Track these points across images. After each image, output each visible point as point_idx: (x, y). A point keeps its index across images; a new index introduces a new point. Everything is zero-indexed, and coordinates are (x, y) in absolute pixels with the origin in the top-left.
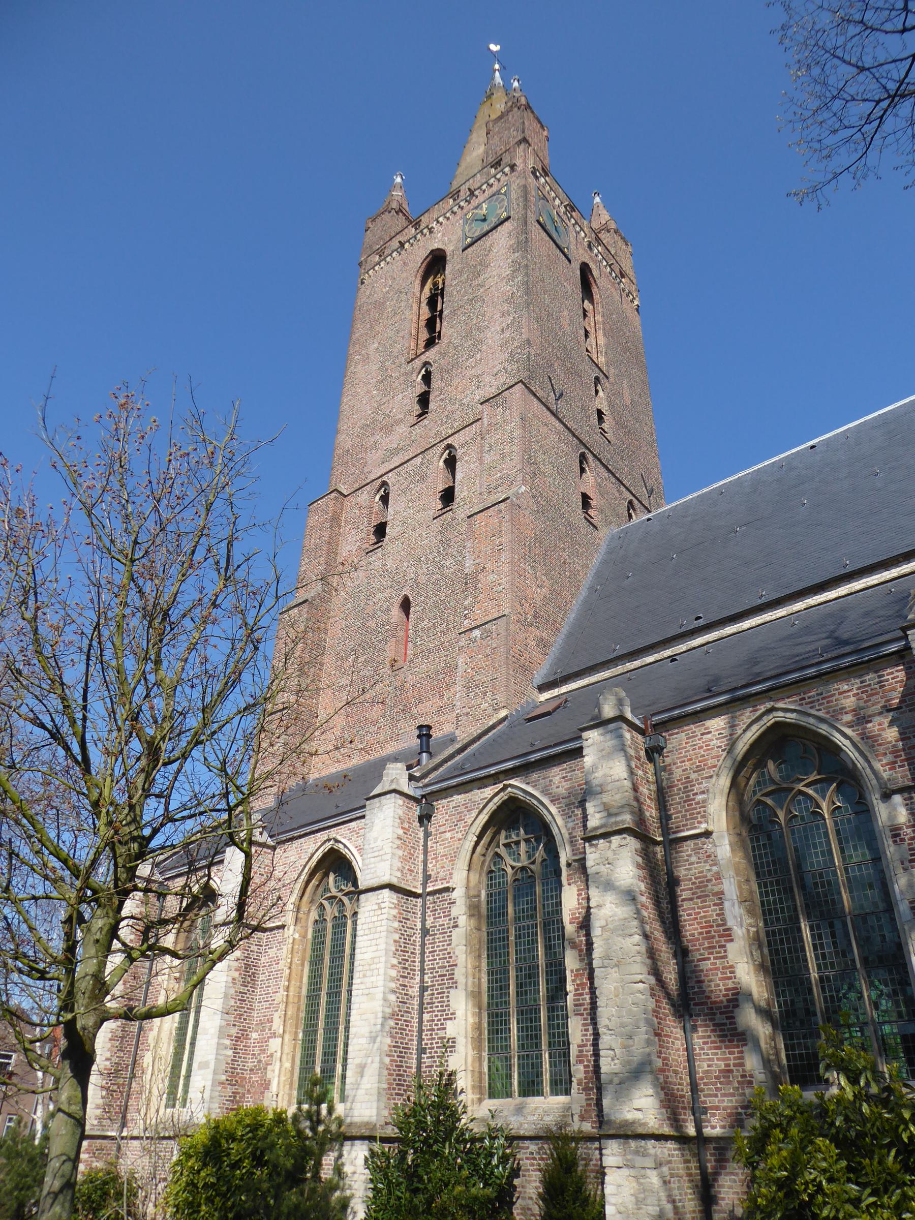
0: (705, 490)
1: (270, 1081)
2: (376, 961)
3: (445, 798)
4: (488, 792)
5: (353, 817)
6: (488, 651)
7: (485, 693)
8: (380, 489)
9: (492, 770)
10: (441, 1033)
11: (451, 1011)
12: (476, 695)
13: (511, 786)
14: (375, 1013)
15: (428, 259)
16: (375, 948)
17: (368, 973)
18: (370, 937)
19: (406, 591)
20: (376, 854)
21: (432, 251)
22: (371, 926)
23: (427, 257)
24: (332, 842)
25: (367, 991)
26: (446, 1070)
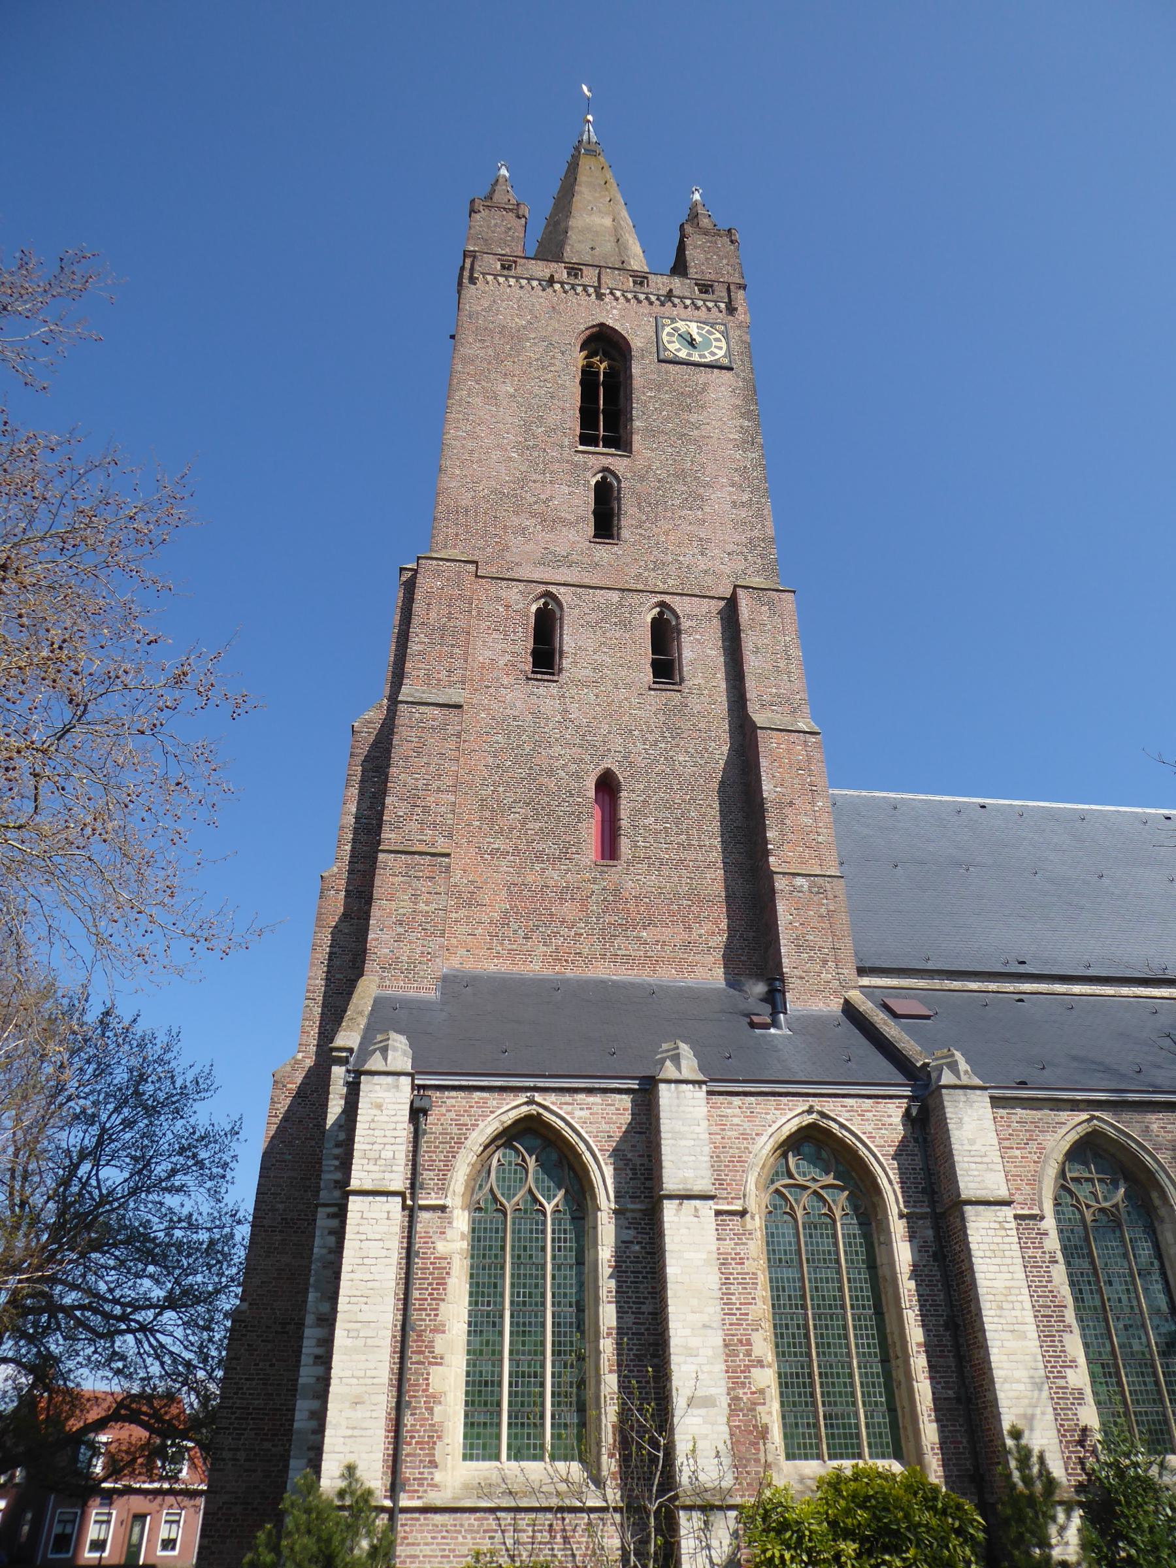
0: (910, 796)
1: (767, 1428)
2: (1014, 1291)
3: (1004, 1108)
4: (1085, 1116)
5: (852, 1092)
6: (823, 910)
7: (825, 962)
8: (540, 598)
9: (1079, 1096)
10: (1062, 1382)
11: (1069, 1358)
12: (811, 958)
13: (1098, 1118)
14: (1035, 1355)
15: (594, 330)
16: (1009, 1276)
17: (1005, 1305)
18: (998, 1261)
19: (607, 763)
20: (979, 1160)
21: (602, 325)
22: (993, 1247)
23: (594, 326)
24: (814, 1116)
25: (1011, 1327)
26: (1077, 1425)
